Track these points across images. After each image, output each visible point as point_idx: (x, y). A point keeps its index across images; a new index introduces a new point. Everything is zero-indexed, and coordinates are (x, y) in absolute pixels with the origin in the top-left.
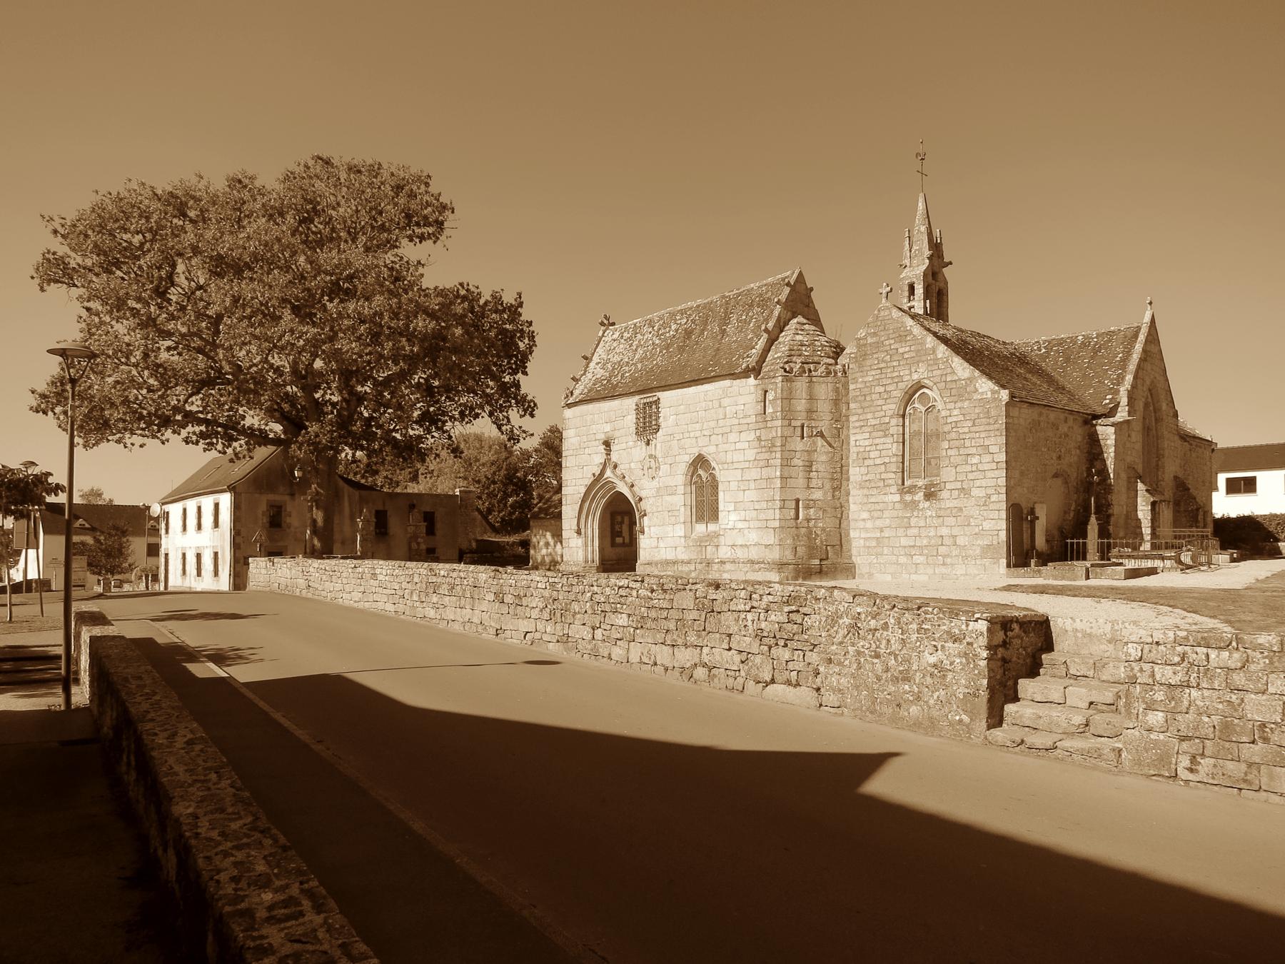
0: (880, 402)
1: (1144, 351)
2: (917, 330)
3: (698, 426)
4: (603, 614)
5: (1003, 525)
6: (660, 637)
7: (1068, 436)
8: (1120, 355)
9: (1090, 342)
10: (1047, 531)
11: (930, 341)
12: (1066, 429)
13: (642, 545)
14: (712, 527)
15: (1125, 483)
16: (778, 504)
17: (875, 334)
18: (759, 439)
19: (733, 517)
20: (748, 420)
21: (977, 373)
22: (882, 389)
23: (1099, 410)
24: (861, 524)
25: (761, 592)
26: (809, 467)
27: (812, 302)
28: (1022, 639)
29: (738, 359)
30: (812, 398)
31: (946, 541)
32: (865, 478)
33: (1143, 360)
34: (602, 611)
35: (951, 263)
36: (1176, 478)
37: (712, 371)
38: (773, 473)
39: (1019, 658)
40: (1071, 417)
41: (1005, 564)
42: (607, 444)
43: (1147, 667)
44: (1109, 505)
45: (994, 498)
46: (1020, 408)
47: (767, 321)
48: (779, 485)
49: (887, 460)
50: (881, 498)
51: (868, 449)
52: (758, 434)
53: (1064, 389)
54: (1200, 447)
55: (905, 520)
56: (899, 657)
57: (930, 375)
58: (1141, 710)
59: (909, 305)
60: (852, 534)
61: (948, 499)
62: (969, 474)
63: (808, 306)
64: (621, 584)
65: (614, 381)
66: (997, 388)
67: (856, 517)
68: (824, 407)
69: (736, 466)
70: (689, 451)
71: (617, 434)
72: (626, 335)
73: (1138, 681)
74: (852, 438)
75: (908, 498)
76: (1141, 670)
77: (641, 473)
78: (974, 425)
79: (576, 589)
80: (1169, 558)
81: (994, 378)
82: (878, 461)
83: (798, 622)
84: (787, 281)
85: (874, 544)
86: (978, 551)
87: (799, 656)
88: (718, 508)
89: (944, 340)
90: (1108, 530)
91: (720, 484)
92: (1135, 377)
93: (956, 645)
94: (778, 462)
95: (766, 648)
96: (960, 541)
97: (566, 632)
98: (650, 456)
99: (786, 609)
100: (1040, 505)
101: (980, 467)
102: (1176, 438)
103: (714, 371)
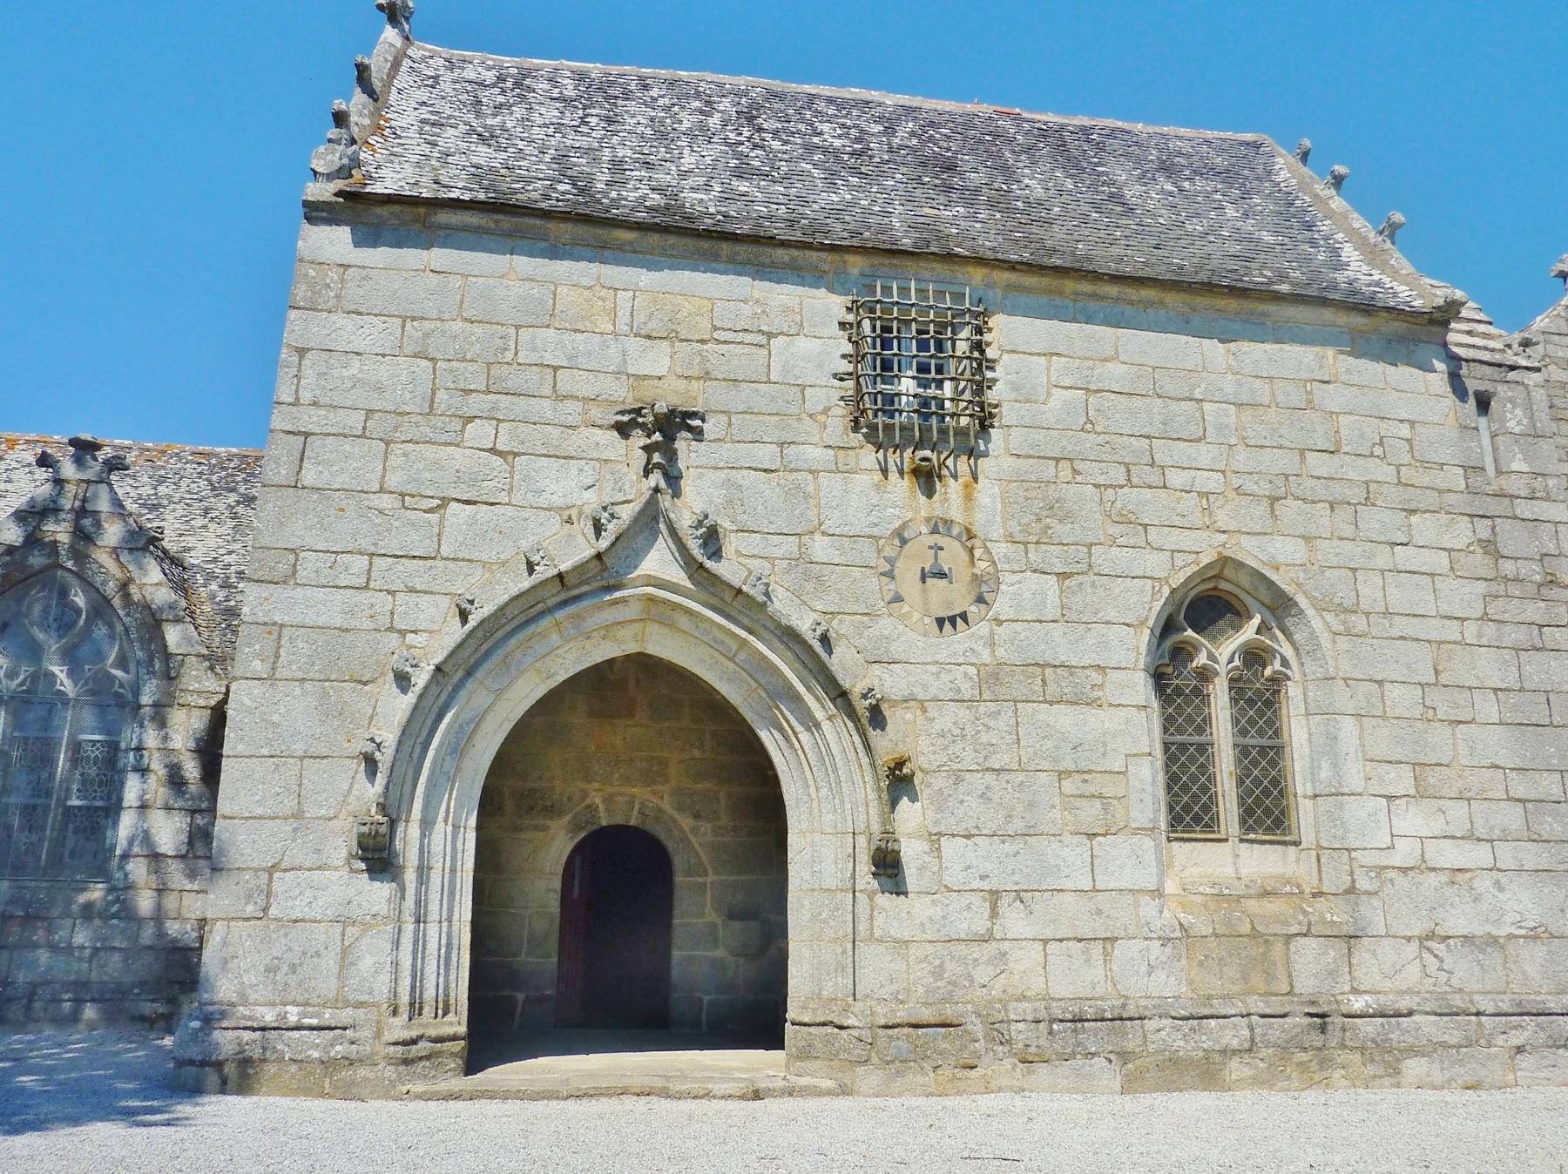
20: (1439, 479)
52: (1484, 533)
69: (1402, 626)
98: (939, 526)
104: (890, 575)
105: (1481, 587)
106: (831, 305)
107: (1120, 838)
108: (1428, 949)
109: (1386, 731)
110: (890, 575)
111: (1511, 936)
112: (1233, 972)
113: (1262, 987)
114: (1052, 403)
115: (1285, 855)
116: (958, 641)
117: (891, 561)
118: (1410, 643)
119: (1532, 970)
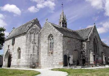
5: (62, 58)
19: (22, 57)
26: (34, 49)
30: (34, 37)
42: (9, 46)
61: (54, 54)
68: (37, 39)
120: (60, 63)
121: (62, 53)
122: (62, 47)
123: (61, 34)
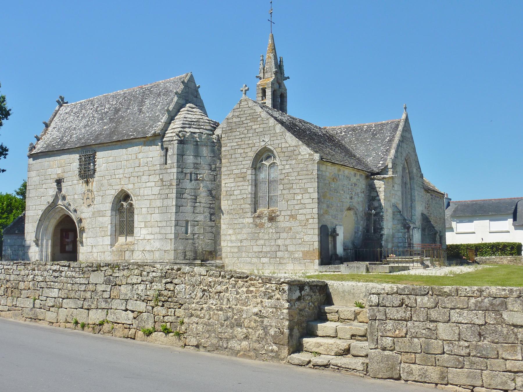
0: (241, 159)
1: (402, 136)
2: (264, 114)
3: (121, 171)
4: (41, 290)
6: (80, 303)
7: (356, 185)
8: (388, 138)
9: (371, 130)
10: (344, 243)
11: (272, 121)
12: (355, 181)
13: (81, 251)
14: (129, 239)
15: (391, 215)
16: (173, 223)
17: (238, 117)
18: (162, 180)
19: (144, 231)
20: (155, 168)
21: (300, 143)
22: (242, 151)
23: (376, 170)
24: (228, 238)
25: (148, 271)
27: (199, 95)
28: (311, 296)
29: (149, 128)
31: (282, 248)
32: (230, 208)
33: (401, 141)
34: (41, 288)
35: (288, 78)
36: (423, 214)
37: (132, 135)
38: (171, 203)
39: (309, 309)
40: (359, 173)
41: (318, 263)
42: (59, 182)
43: (381, 308)
44: (382, 229)
45: (311, 221)
46: (326, 166)
47: (169, 104)
48: (174, 211)
49: (245, 196)
50: (241, 220)
51: (233, 189)
52: (161, 177)
53: (355, 156)
54: (438, 197)
55: (256, 235)
56: (235, 310)
57: (272, 143)
58: (379, 337)
59: (262, 102)
60: (223, 244)
61: (283, 222)
62: (296, 206)
63: (196, 97)
64: (54, 268)
65: (65, 140)
66: (312, 153)
67: (225, 233)
69: (146, 197)
70: (114, 187)
71: (65, 175)
72: (75, 110)
73: (377, 318)
74: (223, 182)
75: (258, 221)
76: (379, 311)
77: (82, 201)
78: (298, 175)
79: (23, 273)
80: (417, 262)
81: (311, 147)
82: (239, 197)
83: (171, 289)
84: (182, 80)
85: (236, 250)
86: (301, 255)
87: (171, 312)
88: (133, 226)
89: (282, 123)
90: (381, 244)
91: (135, 210)
92: (397, 152)
93: (270, 300)
94: (174, 195)
95: (150, 308)
96: (290, 248)
97: (14, 304)
98: (88, 190)
99: (164, 281)
100: (340, 227)
101: (302, 201)
102: (422, 190)
103: (133, 135)
104: (83, 199)
105: (159, 188)
106: (77, 156)
107: (106, 237)
108: (143, 253)
109: (141, 217)
110: (83, 199)
111: (155, 250)
112: (118, 256)
113: (121, 259)
114: (103, 167)
115: (133, 238)
116: (91, 208)
117: (83, 197)
118: (147, 200)
119: (157, 256)
120: (306, 255)
121: (316, 221)
122: (316, 201)
123: (310, 155)
